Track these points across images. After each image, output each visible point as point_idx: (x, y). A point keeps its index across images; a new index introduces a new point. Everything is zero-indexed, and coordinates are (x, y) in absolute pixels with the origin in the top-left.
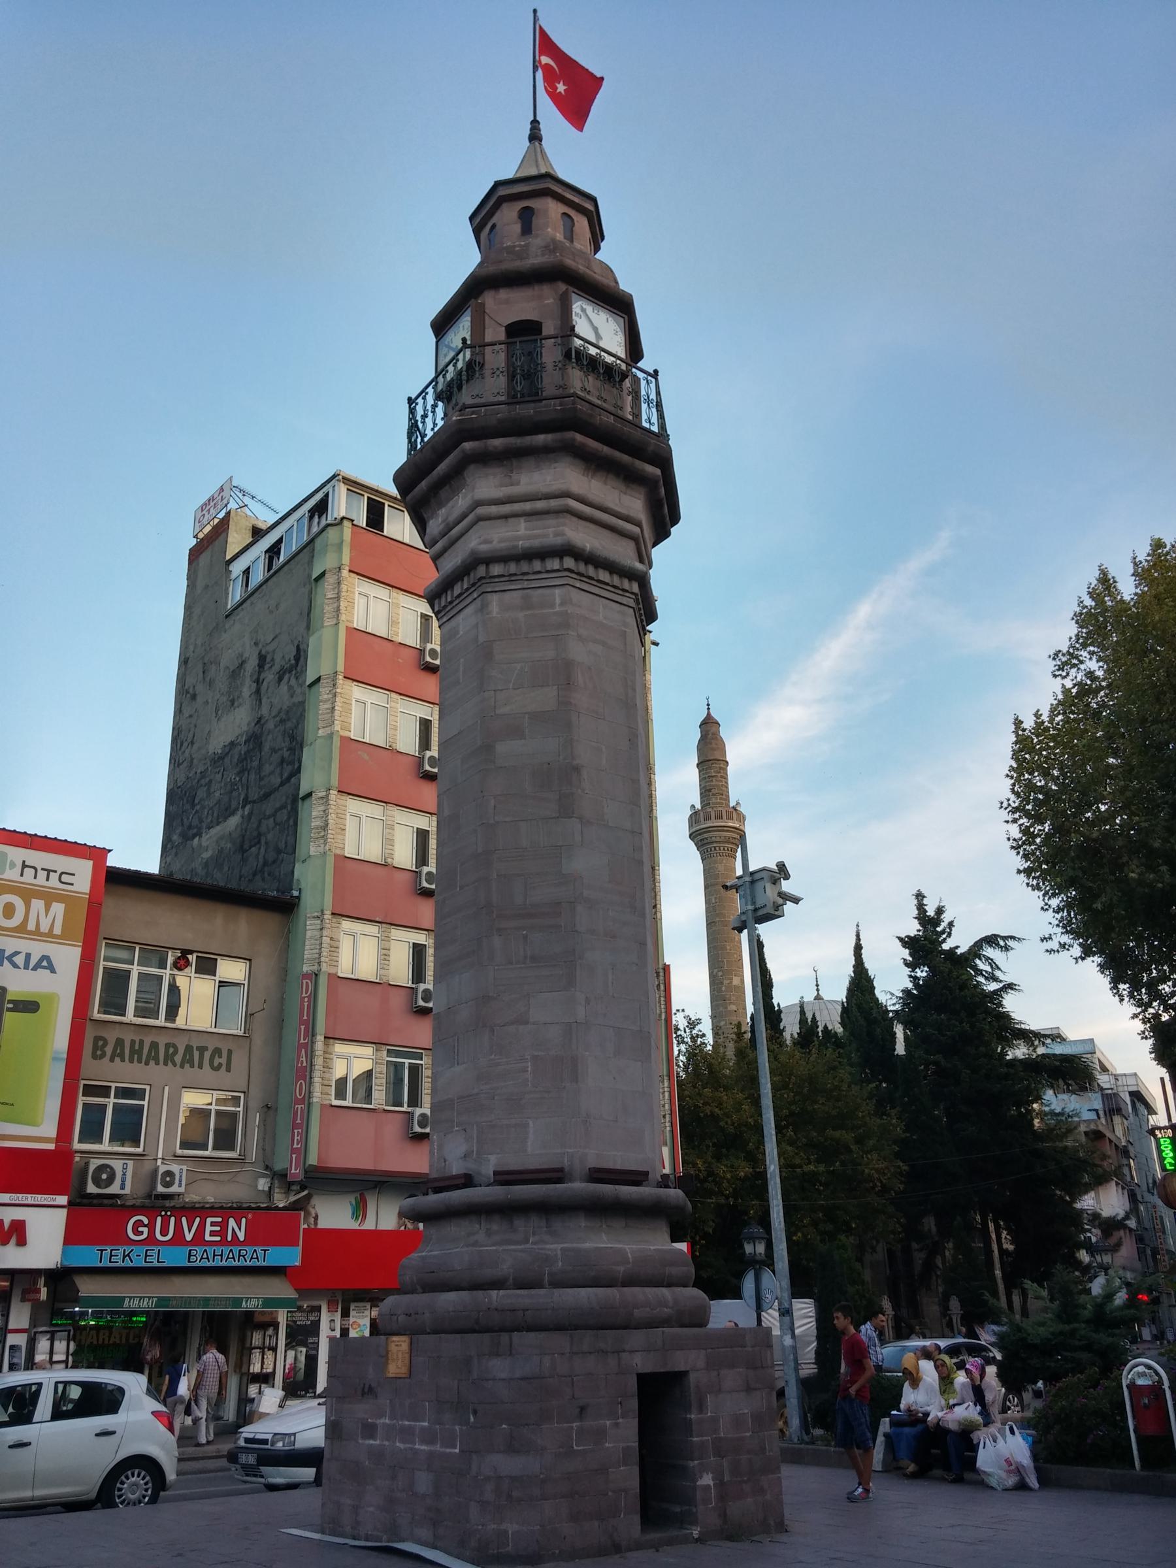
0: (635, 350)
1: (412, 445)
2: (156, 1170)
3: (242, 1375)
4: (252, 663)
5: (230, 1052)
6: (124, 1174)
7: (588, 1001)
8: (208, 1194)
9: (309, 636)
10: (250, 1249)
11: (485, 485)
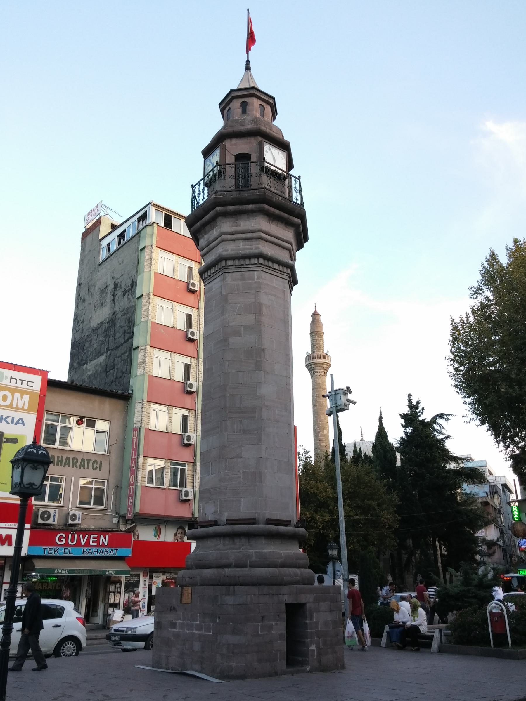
0: (290, 165)
1: (193, 206)
2: (68, 513)
3: (105, 604)
4: (111, 287)
5: (101, 462)
6: (54, 515)
7: (267, 449)
8: (91, 524)
9: (137, 276)
10: (109, 549)
11: (226, 226)
